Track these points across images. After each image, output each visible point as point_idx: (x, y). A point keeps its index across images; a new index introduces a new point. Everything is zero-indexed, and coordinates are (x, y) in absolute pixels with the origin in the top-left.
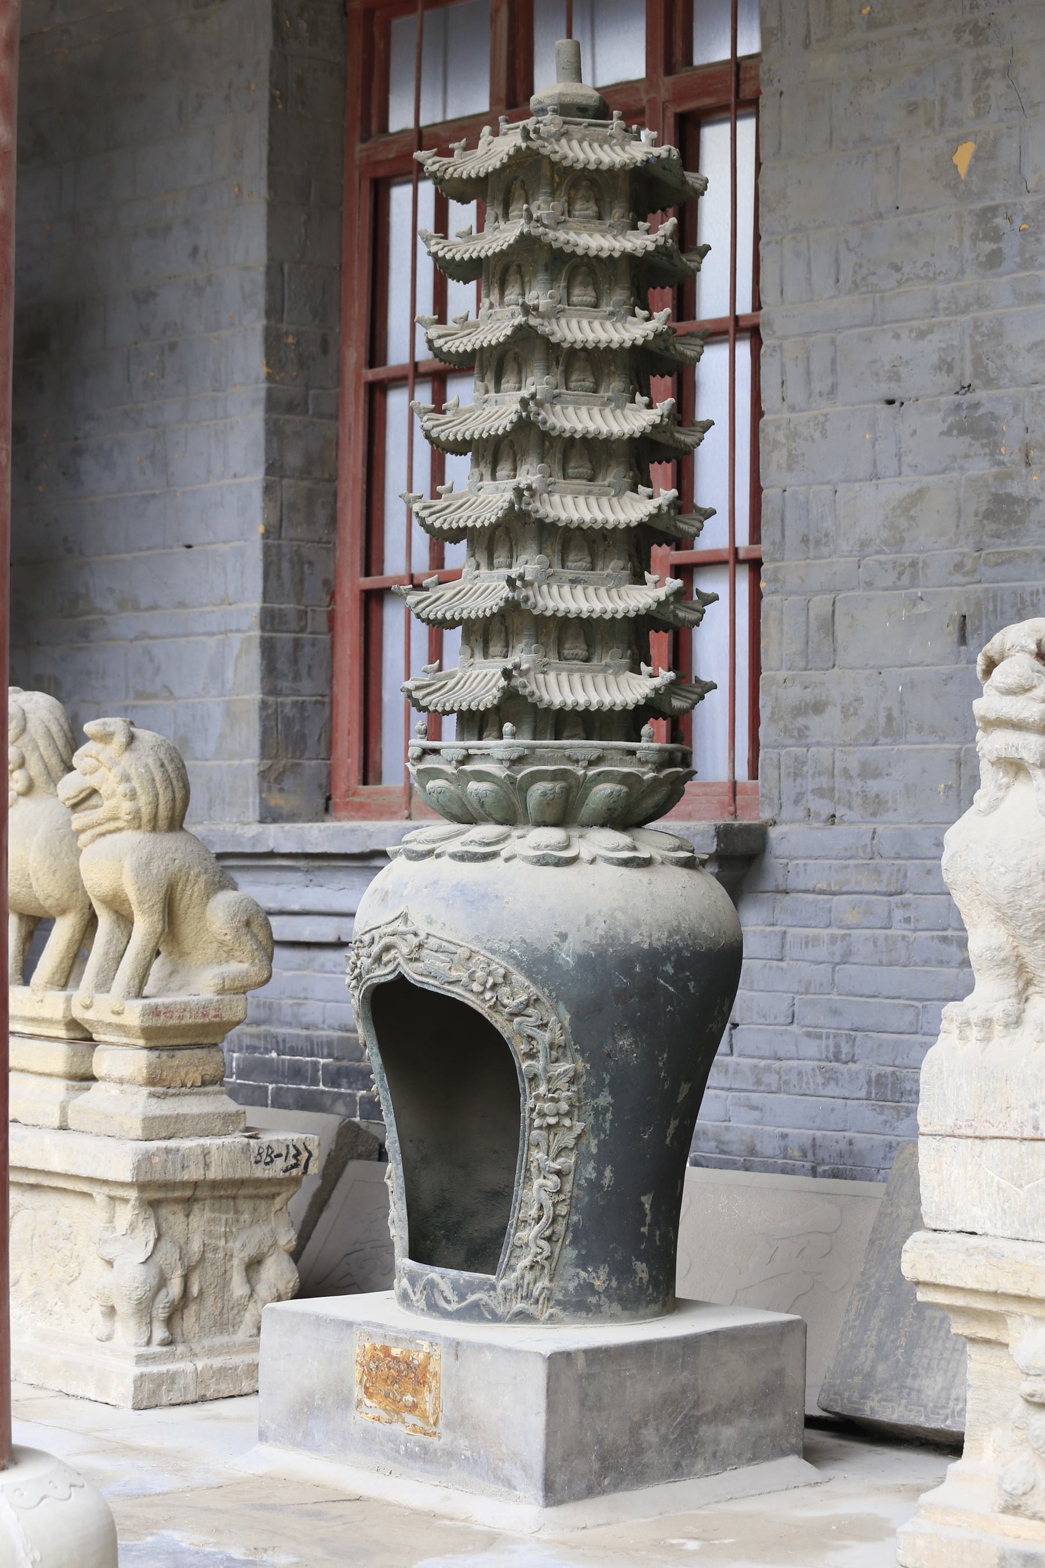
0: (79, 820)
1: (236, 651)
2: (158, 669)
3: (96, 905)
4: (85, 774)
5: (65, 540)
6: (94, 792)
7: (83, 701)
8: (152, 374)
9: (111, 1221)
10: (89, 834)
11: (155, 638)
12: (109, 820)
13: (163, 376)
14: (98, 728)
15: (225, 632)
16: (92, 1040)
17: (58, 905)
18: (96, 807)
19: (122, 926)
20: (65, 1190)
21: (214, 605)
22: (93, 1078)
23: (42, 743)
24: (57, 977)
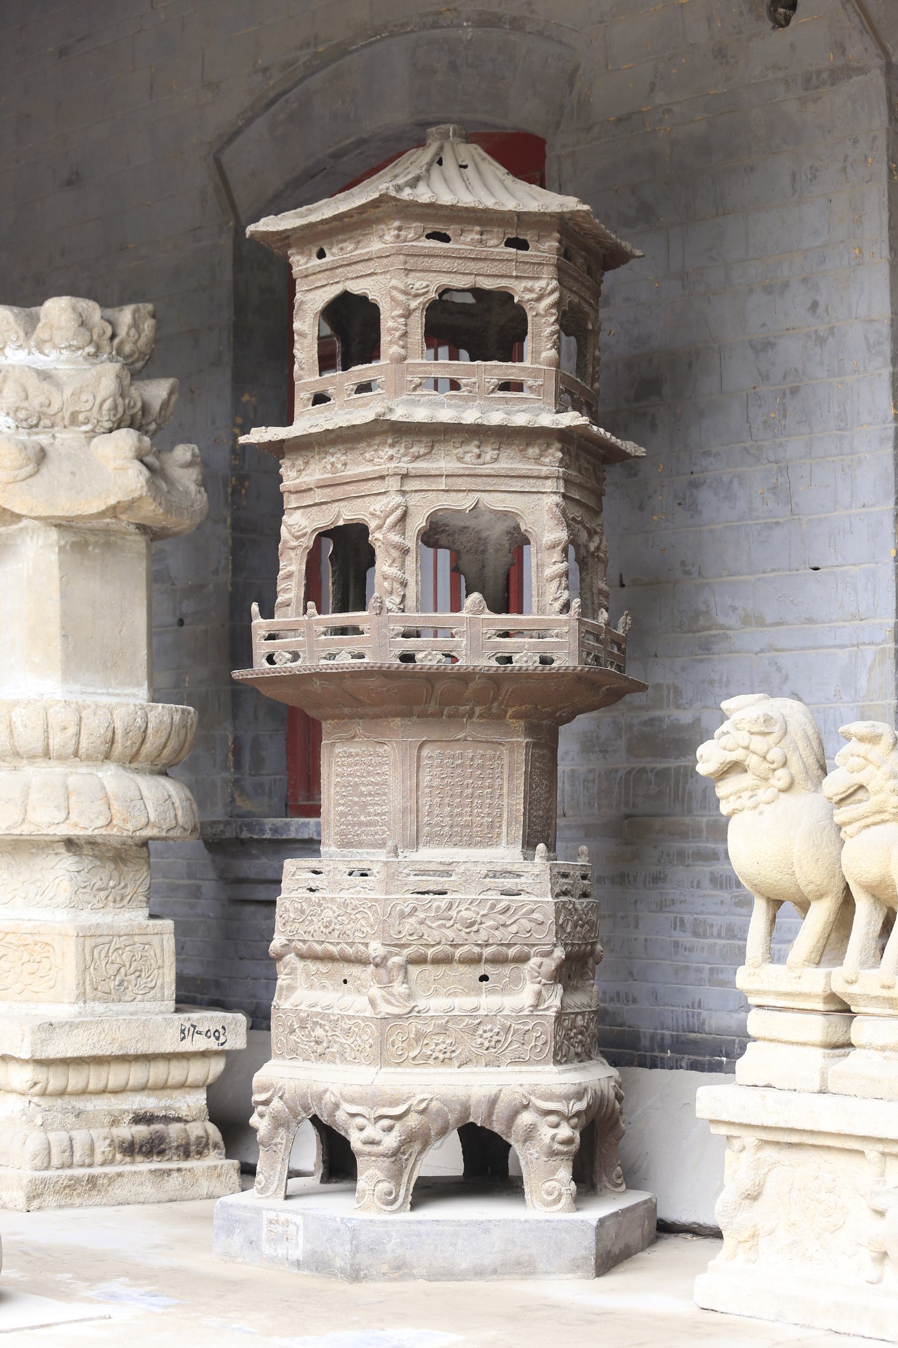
0: (841, 815)
1: (869, 662)
2: (786, 678)
3: (853, 888)
4: (852, 772)
5: (683, 563)
6: (861, 787)
7: (706, 707)
8: (773, 415)
9: (882, 1174)
10: (856, 825)
11: (783, 650)
12: (875, 813)
13: (785, 417)
14: (868, 730)
15: (858, 645)
16: (850, 1011)
17: (818, 890)
18: (860, 801)
19: (878, 909)
20: (829, 1148)
21: (844, 620)
22: (851, 1045)
23: (801, 744)
24: (814, 955)
